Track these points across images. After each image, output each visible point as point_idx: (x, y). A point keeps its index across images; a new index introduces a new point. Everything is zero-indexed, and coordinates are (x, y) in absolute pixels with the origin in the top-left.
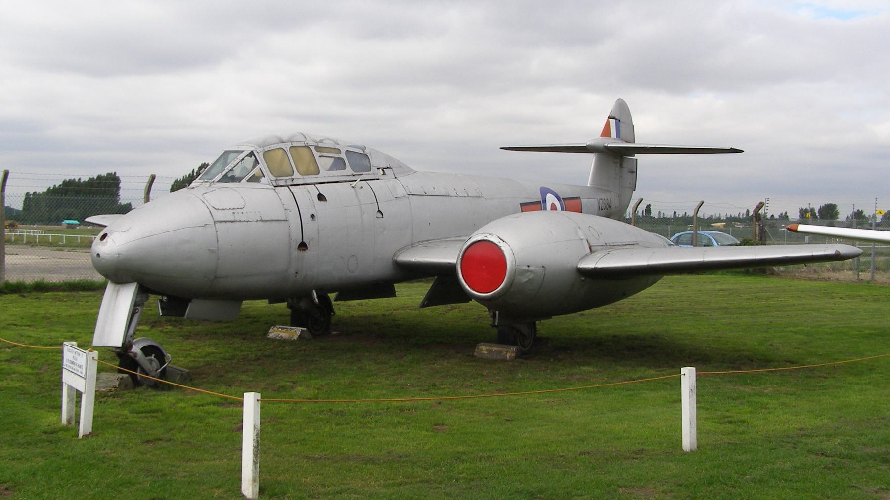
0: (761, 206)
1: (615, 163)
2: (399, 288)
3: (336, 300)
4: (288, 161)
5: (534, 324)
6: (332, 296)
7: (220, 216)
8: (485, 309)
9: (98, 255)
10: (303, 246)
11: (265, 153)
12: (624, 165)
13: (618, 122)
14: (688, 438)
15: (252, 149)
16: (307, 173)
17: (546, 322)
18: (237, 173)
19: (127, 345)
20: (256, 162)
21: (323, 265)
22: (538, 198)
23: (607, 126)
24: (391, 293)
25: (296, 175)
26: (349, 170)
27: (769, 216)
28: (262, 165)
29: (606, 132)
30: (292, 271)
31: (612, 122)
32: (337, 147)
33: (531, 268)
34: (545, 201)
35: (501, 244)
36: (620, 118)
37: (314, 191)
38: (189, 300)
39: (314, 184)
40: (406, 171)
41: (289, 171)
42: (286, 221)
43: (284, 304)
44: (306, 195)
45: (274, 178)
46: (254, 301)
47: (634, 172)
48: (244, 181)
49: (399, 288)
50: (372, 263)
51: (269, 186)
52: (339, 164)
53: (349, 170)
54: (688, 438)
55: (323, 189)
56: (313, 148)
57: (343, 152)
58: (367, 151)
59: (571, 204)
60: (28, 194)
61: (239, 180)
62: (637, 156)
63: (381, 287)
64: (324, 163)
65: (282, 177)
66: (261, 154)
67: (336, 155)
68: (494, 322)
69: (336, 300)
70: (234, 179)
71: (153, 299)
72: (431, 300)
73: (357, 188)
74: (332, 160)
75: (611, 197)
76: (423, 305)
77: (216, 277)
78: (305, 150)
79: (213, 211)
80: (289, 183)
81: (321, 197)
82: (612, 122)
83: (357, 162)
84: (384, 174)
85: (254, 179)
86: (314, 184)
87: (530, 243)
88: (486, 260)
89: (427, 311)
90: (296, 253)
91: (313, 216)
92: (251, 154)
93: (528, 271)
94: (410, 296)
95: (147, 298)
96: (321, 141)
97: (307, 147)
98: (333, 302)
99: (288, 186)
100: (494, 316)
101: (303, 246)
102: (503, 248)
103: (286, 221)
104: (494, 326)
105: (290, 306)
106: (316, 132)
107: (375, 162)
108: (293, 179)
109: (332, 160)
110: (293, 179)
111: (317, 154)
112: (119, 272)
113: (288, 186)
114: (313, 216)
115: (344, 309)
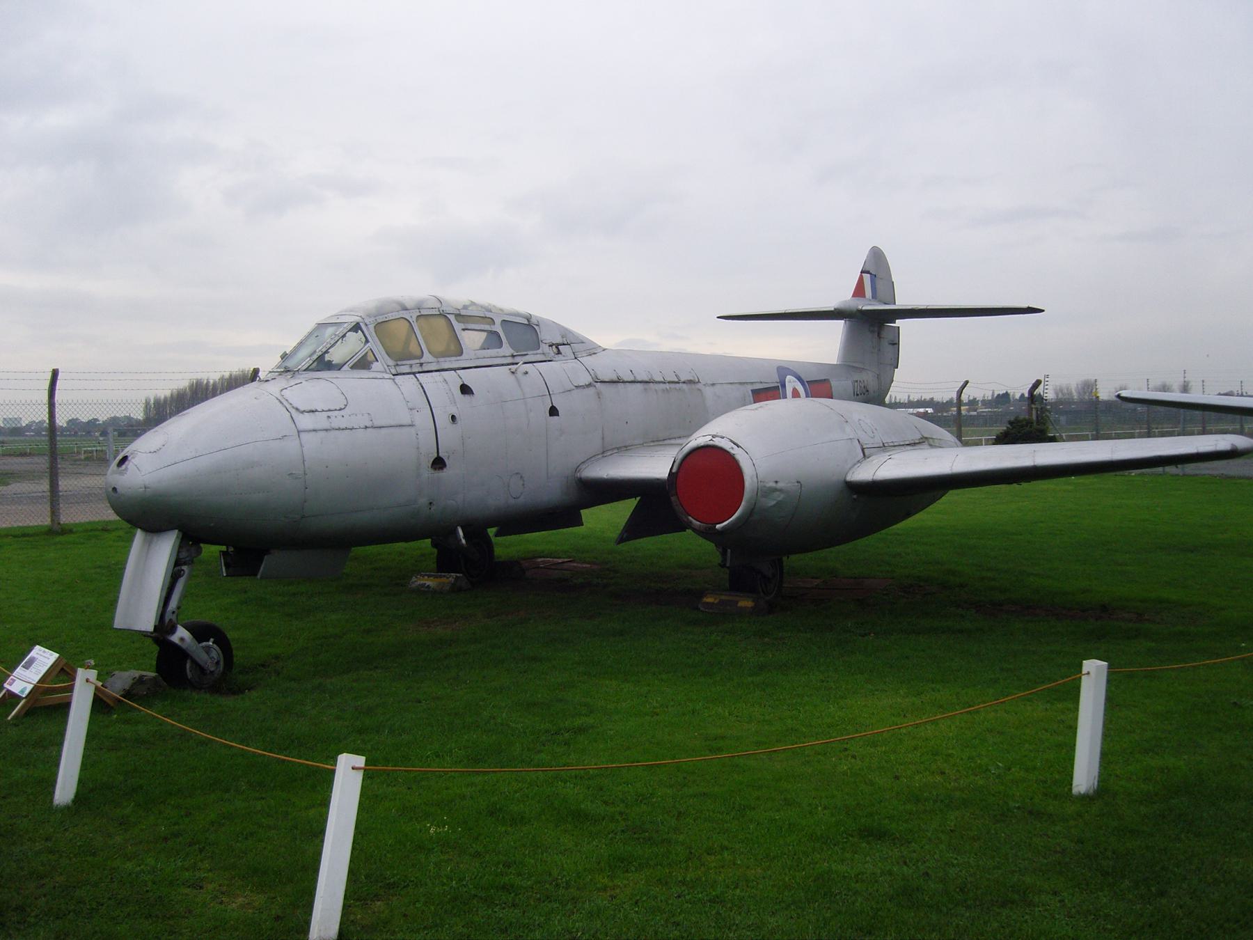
0: (1038, 383)
1: (872, 332)
2: (585, 513)
3: (497, 535)
4: (406, 338)
5: (780, 561)
6: (492, 531)
7: (305, 421)
8: (712, 545)
9: (115, 489)
10: (439, 463)
11: (380, 327)
12: (884, 334)
13: (873, 277)
14: (1084, 773)
15: (358, 319)
16: (445, 354)
17: (793, 557)
18: (336, 356)
19: (164, 627)
20: (367, 341)
21: (474, 487)
22: (773, 380)
23: (860, 283)
24: (579, 522)
25: (427, 357)
26: (506, 350)
27: (1017, 396)
28: (375, 345)
29: (859, 291)
30: (423, 501)
31: (867, 277)
32: (488, 315)
33: (780, 485)
34: (784, 386)
35: (736, 452)
36: (876, 271)
37: (454, 379)
38: (266, 551)
39: (455, 370)
40: (593, 350)
41: (419, 353)
42: (412, 426)
43: (428, 541)
44: (440, 386)
45: (391, 363)
46: (368, 548)
47: (895, 344)
48: (346, 368)
49: (585, 513)
50: (543, 483)
51: (387, 376)
52: (494, 340)
53: (506, 350)
54: (1084, 773)
55: (469, 377)
56: (452, 318)
57: (498, 321)
58: (533, 321)
59: (818, 387)
60: (147, 403)
61: (339, 367)
62: (899, 323)
63: (561, 515)
64: (472, 340)
65: (404, 358)
66: (371, 327)
67: (487, 327)
68: (724, 560)
69: (497, 535)
70: (329, 366)
71: (211, 551)
72: (634, 529)
73: (519, 374)
74: (484, 335)
75: (868, 378)
76: (621, 540)
77: (303, 517)
78: (442, 321)
79: (293, 411)
80: (415, 369)
81: (465, 390)
82: (867, 277)
83: (522, 336)
84: (559, 353)
85: (363, 364)
86: (455, 370)
87: (774, 447)
88: (712, 470)
89: (624, 547)
90: (427, 473)
91: (453, 418)
92: (356, 328)
93: (775, 490)
94: (606, 520)
95: (199, 551)
96: (465, 307)
97: (443, 315)
98: (494, 540)
99: (414, 374)
100: (724, 554)
101: (439, 463)
102: (738, 457)
103: (412, 426)
104: (723, 565)
105: (434, 545)
106: (458, 294)
107: (546, 336)
108: (421, 364)
109: (484, 335)
110: (421, 364)
111: (458, 326)
112: (146, 514)
113: (414, 374)
114: (453, 418)
115: (506, 546)
